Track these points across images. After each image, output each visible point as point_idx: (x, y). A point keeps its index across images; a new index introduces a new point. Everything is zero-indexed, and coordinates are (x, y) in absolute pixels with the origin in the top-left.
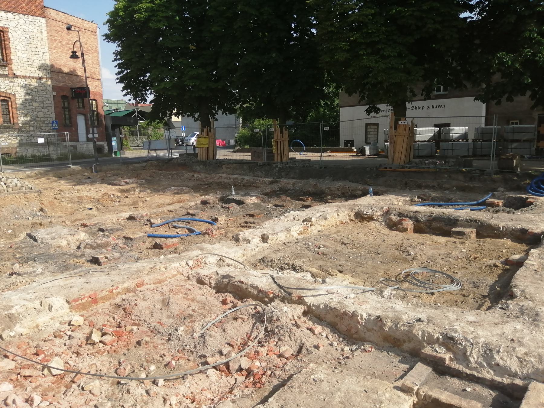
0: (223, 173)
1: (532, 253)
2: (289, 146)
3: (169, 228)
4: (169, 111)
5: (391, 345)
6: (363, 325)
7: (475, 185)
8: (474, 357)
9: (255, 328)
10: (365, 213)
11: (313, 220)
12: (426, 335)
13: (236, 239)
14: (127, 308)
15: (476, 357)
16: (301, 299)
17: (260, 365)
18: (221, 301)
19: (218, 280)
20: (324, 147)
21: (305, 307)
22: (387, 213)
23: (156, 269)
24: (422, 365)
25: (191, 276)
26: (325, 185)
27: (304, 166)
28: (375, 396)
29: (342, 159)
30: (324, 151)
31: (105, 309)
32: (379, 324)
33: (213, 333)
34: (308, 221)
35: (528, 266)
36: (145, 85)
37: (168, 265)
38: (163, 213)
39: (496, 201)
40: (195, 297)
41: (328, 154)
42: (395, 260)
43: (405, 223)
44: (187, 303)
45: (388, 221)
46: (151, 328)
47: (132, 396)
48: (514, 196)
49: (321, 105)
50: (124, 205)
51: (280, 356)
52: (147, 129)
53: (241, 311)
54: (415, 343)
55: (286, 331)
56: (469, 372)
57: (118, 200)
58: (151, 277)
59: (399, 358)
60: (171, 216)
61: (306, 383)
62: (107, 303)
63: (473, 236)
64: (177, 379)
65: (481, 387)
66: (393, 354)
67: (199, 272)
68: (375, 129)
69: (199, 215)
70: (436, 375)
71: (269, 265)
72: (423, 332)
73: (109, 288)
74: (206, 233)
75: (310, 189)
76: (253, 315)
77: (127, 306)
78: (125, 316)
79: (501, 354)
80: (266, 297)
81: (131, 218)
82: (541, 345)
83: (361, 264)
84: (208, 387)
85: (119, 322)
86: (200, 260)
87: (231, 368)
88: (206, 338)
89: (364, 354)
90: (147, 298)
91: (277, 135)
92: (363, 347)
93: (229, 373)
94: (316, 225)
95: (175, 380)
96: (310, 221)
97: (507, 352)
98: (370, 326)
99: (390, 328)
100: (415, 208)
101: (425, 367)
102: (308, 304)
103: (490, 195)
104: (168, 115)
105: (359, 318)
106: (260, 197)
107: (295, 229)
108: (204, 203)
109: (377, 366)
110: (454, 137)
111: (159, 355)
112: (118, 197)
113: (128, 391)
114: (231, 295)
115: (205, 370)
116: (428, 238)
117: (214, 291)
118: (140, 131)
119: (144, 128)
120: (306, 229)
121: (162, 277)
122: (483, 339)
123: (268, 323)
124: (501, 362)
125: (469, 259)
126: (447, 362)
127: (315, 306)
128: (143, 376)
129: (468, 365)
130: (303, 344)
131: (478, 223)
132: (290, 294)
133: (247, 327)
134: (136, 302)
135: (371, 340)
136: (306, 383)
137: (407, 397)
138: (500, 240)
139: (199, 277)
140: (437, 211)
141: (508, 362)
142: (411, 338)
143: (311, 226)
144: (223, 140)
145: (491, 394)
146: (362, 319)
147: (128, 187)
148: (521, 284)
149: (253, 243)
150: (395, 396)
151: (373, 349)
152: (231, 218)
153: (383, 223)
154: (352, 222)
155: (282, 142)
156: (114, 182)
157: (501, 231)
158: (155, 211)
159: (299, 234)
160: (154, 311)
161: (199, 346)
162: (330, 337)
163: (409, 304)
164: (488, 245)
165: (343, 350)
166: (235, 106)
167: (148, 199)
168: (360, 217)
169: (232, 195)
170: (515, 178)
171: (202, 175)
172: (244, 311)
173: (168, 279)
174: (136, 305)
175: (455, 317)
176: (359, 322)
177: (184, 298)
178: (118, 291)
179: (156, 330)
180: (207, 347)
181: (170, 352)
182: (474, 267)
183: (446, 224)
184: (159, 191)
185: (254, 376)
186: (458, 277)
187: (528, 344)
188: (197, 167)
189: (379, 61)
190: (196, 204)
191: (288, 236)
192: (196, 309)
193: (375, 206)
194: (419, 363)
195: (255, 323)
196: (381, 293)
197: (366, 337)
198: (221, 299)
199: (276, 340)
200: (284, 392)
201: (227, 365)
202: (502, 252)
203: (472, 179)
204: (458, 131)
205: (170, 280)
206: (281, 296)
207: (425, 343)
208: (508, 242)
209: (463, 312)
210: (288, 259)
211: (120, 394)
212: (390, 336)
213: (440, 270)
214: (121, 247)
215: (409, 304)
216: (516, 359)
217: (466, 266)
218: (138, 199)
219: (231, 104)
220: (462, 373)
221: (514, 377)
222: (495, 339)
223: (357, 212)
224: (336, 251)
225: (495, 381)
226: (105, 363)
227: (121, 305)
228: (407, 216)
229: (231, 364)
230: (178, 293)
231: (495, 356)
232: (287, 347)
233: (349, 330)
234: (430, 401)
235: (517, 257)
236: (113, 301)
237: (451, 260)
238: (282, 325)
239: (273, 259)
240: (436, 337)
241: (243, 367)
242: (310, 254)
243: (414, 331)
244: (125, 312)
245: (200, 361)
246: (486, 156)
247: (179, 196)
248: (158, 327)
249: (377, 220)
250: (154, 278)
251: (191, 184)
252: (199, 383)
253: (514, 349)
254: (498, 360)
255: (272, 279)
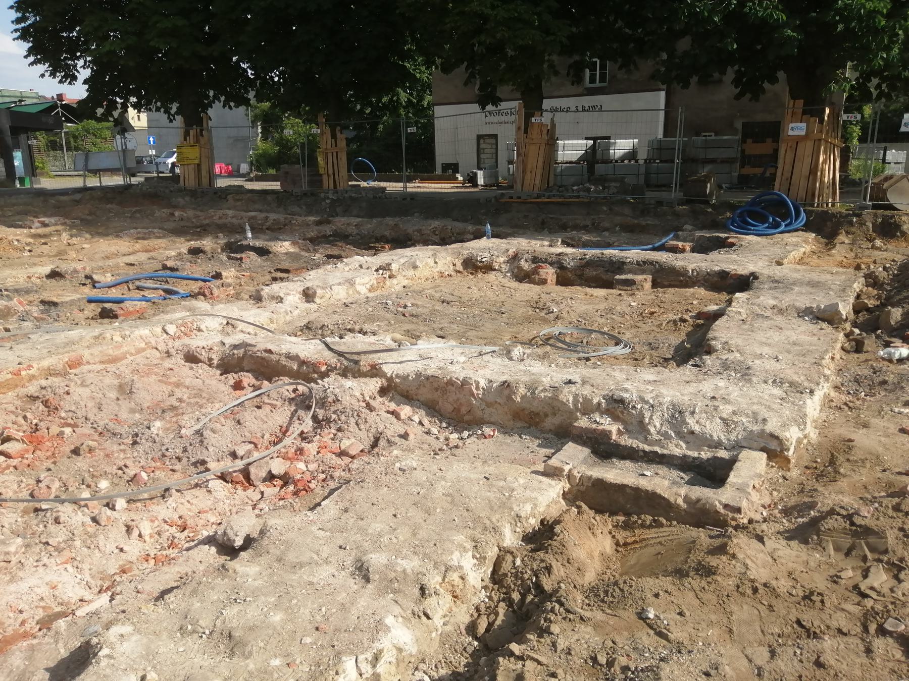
0: (229, 209)
1: (737, 298)
2: (349, 171)
3: (129, 290)
4: (121, 99)
5: (526, 425)
6: (480, 399)
7: (649, 222)
8: (656, 424)
9: (295, 418)
10: (479, 258)
11: (394, 267)
12: (581, 400)
13: (258, 298)
14: (51, 400)
15: (658, 425)
16: (376, 369)
17: (305, 469)
18: (231, 386)
19: (224, 352)
20: (406, 173)
21: (384, 380)
22: (515, 258)
23: (104, 338)
24: (575, 445)
25: (173, 352)
26: (411, 225)
27: (375, 197)
28: (501, 483)
29: (440, 190)
30: (410, 180)
31: (6, 403)
32: (506, 392)
33: (218, 426)
34: (385, 270)
35: (731, 314)
36: (74, 48)
37: (127, 333)
38: (117, 266)
39: (680, 244)
40: (182, 381)
41: (416, 185)
42: (529, 320)
43: (542, 272)
44: (167, 389)
45: (516, 271)
46: (100, 429)
47: (64, 527)
48: (708, 235)
49: (401, 104)
50: (40, 256)
51: (342, 454)
52: (83, 140)
53: (269, 395)
54: (562, 416)
55: (350, 415)
56: (647, 448)
57: (27, 248)
58: (96, 350)
59: (538, 441)
60: (131, 273)
61: (386, 474)
62: (10, 394)
63: (648, 285)
64: (151, 499)
65: (667, 469)
66: (527, 437)
67: (189, 343)
68: (492, 144)
69: (185, 270)
70: (597, 460)
71: (318, 334)
72: (576, 397)
73: (13, 367)
74: (199, 294)
75: (387, 233)
76: (291, 400)
77: (49, 396)
78: (47, 413)
79: (697, 416)
80: (315, 372)
81: (55, 275)
82: (756, 401)
83: (475, 327)
84: (212, 507)
85: (36, 425)
86: (190, 325)
87: (252, 477)
88: (204, 433)
89: (483, 440)
90: (88, 382)
91: (326, 142)
92: (479, 432)
93: (250, 485)
94: (399, 277)
95: (147, 502)
96: (389, 269)
97: (706, 413)
98: (490, 399)
99: (523, 397)
100: (560, 249)
101: (580, 448)
102: (389, 375)
103: (671, 236)
104: (119, 106)
105: (473, 388)
106: (298, 243)
107: (363, 281)
108: (195, 252)
109: (503, 453)
110: (616, 157)
111: (115, 467)
112: (28, 244)
113: (57, 521)
114: (250, 375)
115: (204, 482)
116: (579, 292)
117: (218, 372)
118: (68, 143)
119: (75, 137)
120: (381, 282)
121: (117, 353)
122: (669, 399)
123: (319, 408)
124: (697, 428)
125: (641, 314)
126: (614, 437)
127: (400, 376)
128: (86, 494)
129: (646, 439)
130: (381, 434)
131: (655, 266)
132: (356, 362)
133: (281, 416)
134: (67, 389)
135: (492, 420)
136: (386, 474)
137: (553, 482)
138: (687, 289)
139: (188, 351)
140: (592, 253)
141: (708, 427)
142: (556, 409)
143: (390, 277)
144: (227, 165)
145: (682, 478)
146: (477, 388)
147: (47, 230)
148: (723, 335)
149: (288, 303)
150: (535, 482)
151: (496, 433)
152: (245, 274)
153: (509, 274)
154: (458, 274)
155: (335, 154)
156: (20, 223)
157: (689, 277)
158: (101, 264)
159: (370, 291)
160: (103, 403)
161: (191, 447)
162: (426, 421)
163: (553, 365)
164: (671, 296)
165: (447, 439)
166: (247, 92)
167: (85, 246)
168: (472, 266)
169: (246, 238)
170: (710, 210)
171: (190, 213)
172: (274, 394)
173: (128, 356)
174: (68, 393)
175: (624, 377)
176: (473, 395)
177: (159, 381)
178: (30, 372)
179: (108, 431)
180: (206, 448)
181: (137, 463)
182: (649, 325)
183: (607, 271)
184: (107, 235)
185: (295, 483)
186: (627, 336)
187: (737, 400)
188: (180, 200)
189: (498, 6)
190: (179, 254)
191: (351, 292)
192: (185, 397)
193: (495, 248)
194: (570, 443)
195: (296, 411)
196: (508, 354)
197: (485, 416)
198: (232, 382)
199: (334, 431)
200: (348, 490)
201: (246, 473)
202: (692, 304)
203: (644, 212)
204: (622, 146)
205: (132, 358)
206: (340, 367)
207: (578, 414)
208: (702, 292)
209: (636, 371)
210: (352, 322)
211: (41, 526)
212: (524, 409)
213: (597, 329)
214: (35, 318)
215: (553, 365)
216: (719, 421)
217: (638, 325)
218: (68, 248)
219: (240, 89)
220: (637, 451)
221: (716, 448)
222: (686, 398)
223: (467, 259)
224: (433, 312)
225: (689, 457)
226: (9, 484)
227: (38, 397)
228: (546, 261)
229: (252, 470)
230: (148, 375)
231: (688, 420)
232: (353, 440)
233: (457, 410)
234: (590, 485)
235: (713, 308)
236: (22, 391)
237: (614, 317)
238: (344, 408)
239: (326, 324)
240: (595, 401)
241: (275, 472)
242: (389, 316)
243: (561, 397)
244: (46, 406)
245: (194, 470)
246: (664, 186)
247: (146, 242)
248: (111, 425)
249: (500, 270)
250: (101, 352)
251: (170, 225)
252: (194, 501)
253: (716, 408)
254: (692, 424)
255: (324, 345)
